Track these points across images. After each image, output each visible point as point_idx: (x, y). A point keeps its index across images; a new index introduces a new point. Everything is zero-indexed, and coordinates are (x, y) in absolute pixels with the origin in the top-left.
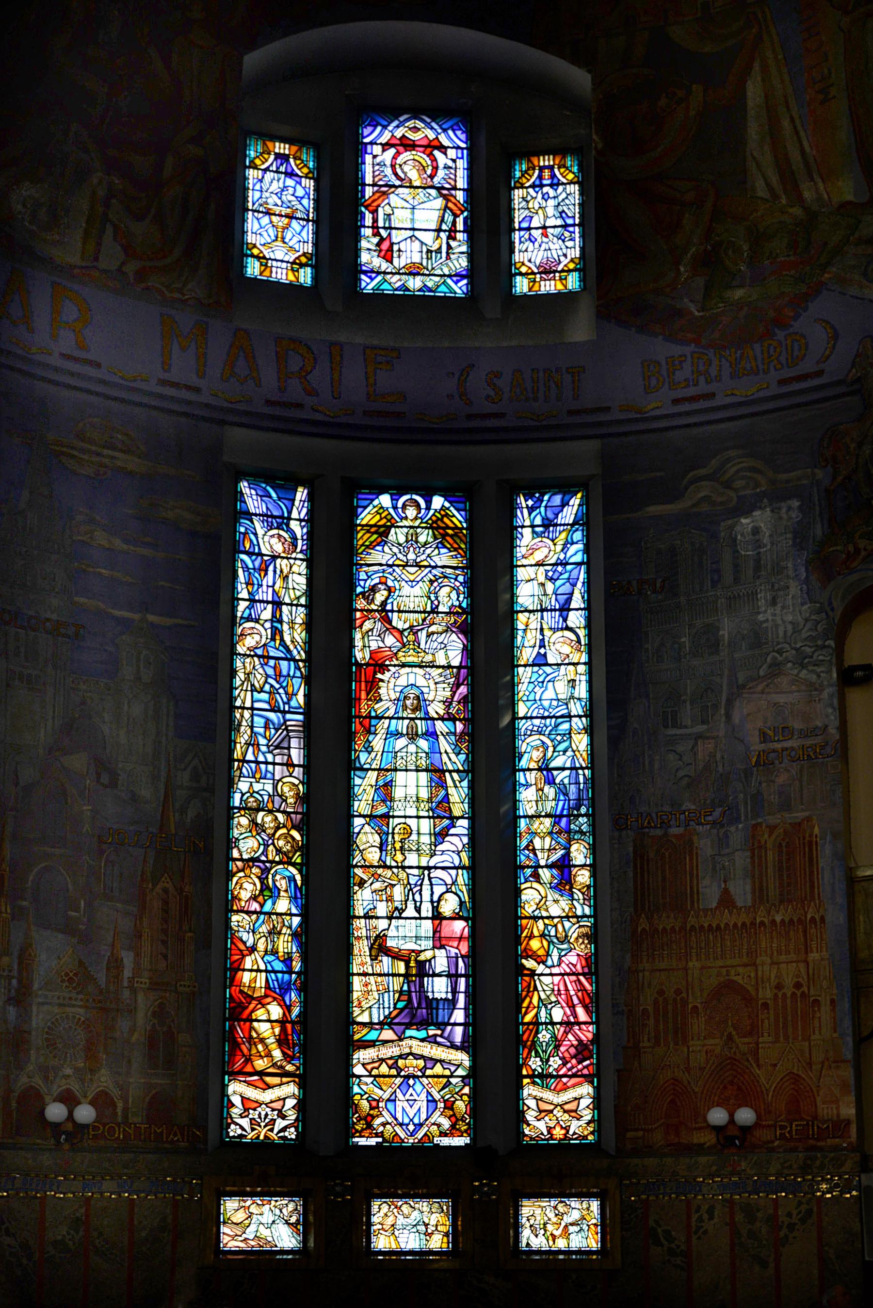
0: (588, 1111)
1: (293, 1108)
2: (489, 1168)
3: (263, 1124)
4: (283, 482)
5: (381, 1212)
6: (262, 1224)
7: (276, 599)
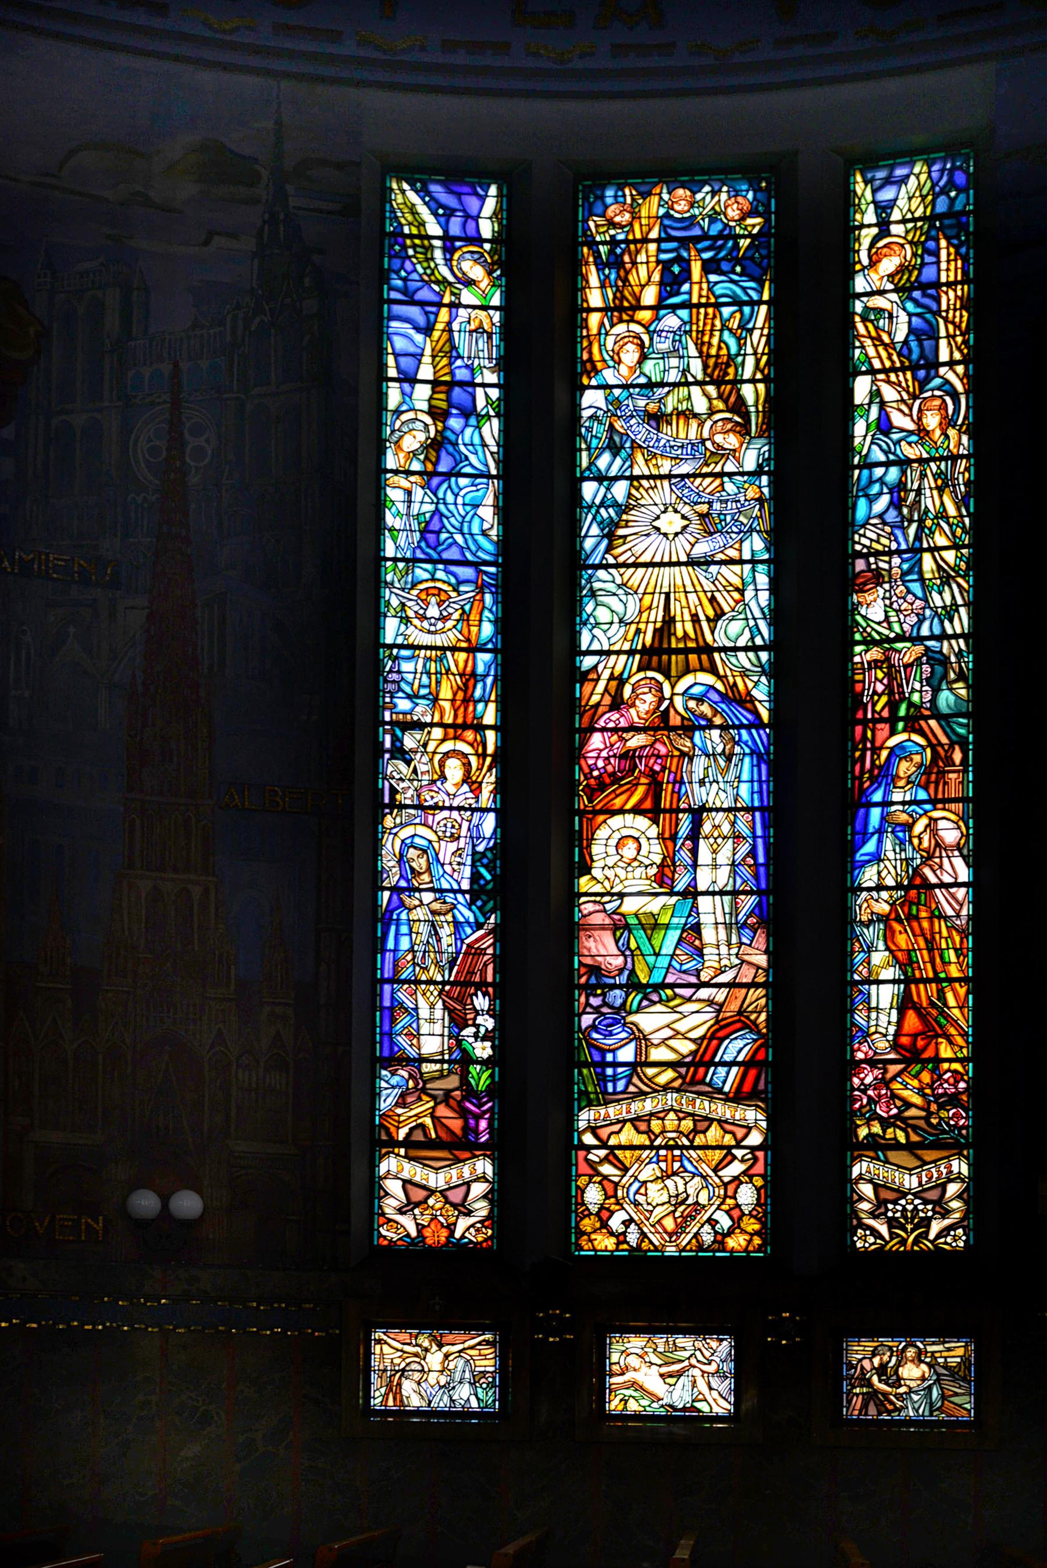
0: (483, 1204)
1: (485, 1197)
2: (790, 1292)
3: (909, 1227)
4: (453, 173)
5: (389, 1349)
6: (435, 1372)
7: (406, 387)
